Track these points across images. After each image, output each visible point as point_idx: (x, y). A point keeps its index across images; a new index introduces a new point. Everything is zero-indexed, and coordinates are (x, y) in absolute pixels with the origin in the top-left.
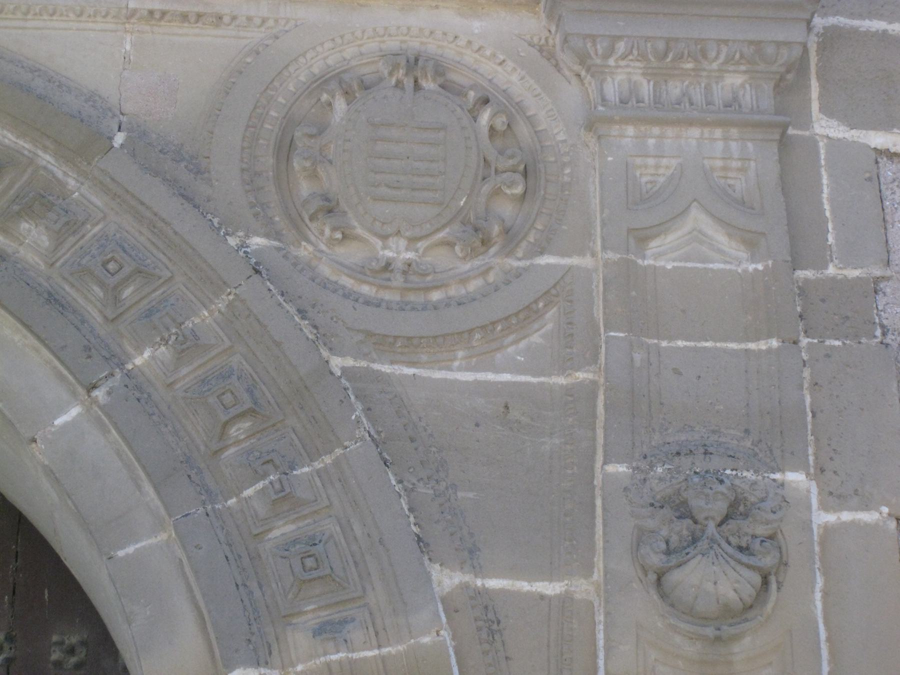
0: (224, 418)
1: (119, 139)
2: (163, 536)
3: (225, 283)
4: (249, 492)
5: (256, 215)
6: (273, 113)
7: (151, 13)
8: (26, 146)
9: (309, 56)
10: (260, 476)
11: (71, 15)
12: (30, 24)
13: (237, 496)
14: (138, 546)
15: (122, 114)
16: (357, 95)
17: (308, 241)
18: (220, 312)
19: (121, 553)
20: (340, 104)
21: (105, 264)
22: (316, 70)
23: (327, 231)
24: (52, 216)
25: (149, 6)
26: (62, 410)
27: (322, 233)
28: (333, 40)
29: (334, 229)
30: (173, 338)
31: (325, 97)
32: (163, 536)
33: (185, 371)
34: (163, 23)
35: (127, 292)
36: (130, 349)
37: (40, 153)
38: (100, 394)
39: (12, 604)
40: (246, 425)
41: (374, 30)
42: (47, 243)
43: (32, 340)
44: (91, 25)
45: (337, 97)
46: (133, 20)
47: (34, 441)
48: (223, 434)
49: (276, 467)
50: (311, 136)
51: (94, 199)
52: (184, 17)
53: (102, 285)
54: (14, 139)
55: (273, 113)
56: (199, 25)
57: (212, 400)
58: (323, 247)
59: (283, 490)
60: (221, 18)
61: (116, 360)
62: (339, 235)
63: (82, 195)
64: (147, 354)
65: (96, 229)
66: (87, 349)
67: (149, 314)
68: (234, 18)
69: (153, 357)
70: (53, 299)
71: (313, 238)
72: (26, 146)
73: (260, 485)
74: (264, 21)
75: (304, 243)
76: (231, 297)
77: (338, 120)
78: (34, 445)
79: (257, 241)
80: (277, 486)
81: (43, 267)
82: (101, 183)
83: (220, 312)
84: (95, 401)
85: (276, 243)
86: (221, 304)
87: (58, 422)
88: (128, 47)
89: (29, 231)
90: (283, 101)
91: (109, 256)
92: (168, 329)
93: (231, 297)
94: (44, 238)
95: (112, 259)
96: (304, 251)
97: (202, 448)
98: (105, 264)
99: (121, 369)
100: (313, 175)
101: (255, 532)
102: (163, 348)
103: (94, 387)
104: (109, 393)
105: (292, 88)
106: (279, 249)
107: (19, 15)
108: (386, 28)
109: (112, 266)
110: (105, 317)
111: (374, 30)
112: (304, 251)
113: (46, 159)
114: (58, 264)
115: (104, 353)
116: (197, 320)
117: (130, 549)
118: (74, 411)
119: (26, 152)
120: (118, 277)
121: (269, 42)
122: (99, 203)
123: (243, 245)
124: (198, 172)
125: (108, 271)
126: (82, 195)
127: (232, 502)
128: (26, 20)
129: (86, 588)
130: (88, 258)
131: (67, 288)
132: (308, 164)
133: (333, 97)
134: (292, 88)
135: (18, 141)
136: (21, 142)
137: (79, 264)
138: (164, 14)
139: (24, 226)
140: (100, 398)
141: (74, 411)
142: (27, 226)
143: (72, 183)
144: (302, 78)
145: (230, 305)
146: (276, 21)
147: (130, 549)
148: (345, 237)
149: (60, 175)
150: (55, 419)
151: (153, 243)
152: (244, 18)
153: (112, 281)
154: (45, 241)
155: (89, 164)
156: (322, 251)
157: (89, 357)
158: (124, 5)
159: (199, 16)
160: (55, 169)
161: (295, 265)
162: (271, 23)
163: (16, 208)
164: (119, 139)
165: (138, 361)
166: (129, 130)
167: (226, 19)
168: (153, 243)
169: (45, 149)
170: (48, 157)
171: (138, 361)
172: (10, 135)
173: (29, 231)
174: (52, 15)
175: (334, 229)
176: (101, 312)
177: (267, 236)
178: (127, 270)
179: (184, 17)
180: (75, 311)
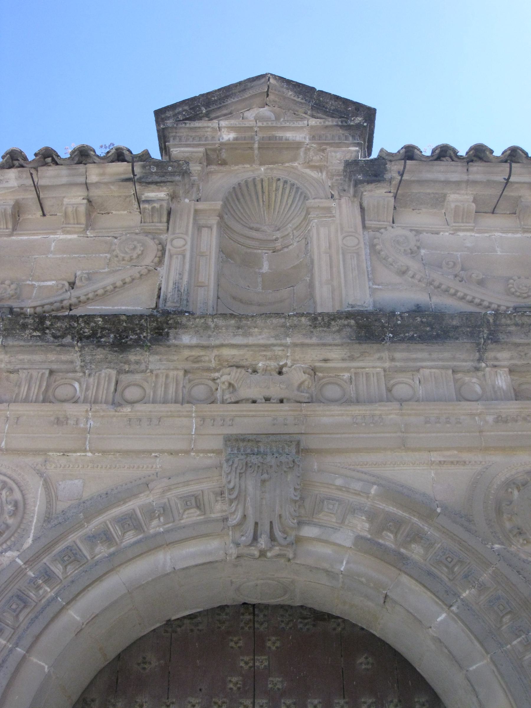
0: (501, 615)
1: (439, 510)
2: (485, 662)
3: (490, 563)
4: (515, 642)
5: (494, 536)
6: (491, 497)
7: (440, 462)
8: (407, 515)
9: (500, 475)
10: (518, 636)
11: (411, 464)
12: (396, 468)
13: (510, 644)
14: (477, 665)
15: (436, 500)
16: (521, 488)
17: (513, 545)
18: (490, 574)
19: (471, 669)
20: (516, 492)
21: (446, 558)
22: (503, 480)
23: (521, 541)
24: (422, 541)
25: (439, 459)
26: (439, 615)
27: (518, 541)
28: (507, 468)
29: (524, 540)
30: (477, 585)
31: (510, 490)
32: (485, 662)
33: (482, 597)
34: (444, 465)
35: (456, 569)
36: (460, 591)
37: (412, 517)
38: (454, 608)
39: (398, 687)
40: (509, 617)
41: (521, 463)
42: (423, 552)
43: (423, 589)
44: (418, 468)
45: (515, 490)
46: (433, 465)
47: (431, 627)
48: (501, 621)
49: (524, 633)
50: (508, 505)
51: (436, 534)
52: (452, 463)
53: (447, 567)
54: (402, 513)
55: (491, 497)
56: (458, 465)
57: (496, 608)
58: (519, 547)
59: (528, 641)
60: (465, 462)
61: (457, 595)
62: (525, 542)
63: (431, 533)
64: (467, 592)
65: (439, 545)
66: (446, 591)
67: (466, 576)
68: (470, 462)
69: (470, 593)
70: (430, 574)
71: (515, 543)
72: (407, 515)
73: (519, 640)
74: (481, 462)
75: (513, 546)
76: (494, 569)
77: (516, 498)
78: (430, 629)
79: (497, 546)
80: (526, 639)
81: (422, 561)
82: (438, 528)
83: (490, 574)
84: (452, 612)
85: (503, 546)
86: (490, 571)
87: (439, 620)
88: (433, 475)
89: (415, 548)
90: (494, 492)
91: (448, 556)
92: (474, 582)
93: (494, 569)
94: (422, 550)
95: (449, 557)
96: (513, 549)
97: (494, 627)
98: (446, 558)
99: (460, 598)
100: (510, 520)
101: (520, 657)
102: (473, 590)
103: (451, 606)
104: (458, 608)
105: (495, 487)
106: (505, 549)
107: (392, 465)
108: (525, 463)
109: (449, 560)
110: (449, 579)
111: (521, 463)
112: (513, 549)
113: (415, 520)
114: (428, 560)
115: (453, 593)
116: (483, 578)
117: (474, 667)
118: (444, 615)
119: (407, 518)
120: (452, 563)
121: (484, 470)
122: (438, 535)
123: (492, 548)
124: (470, 521)
125: (447, 561)
126: (431, 533)
127: (509, 646)
128: (394, 467)
129: (429, 681)
130: (439, 556)
131: (433, 569)
132: (509, 516)
133: (513, 490)
134: (495, 487)
135: (403, 514)
136: (404, 514)
137: (436, 559)
138: (444, 462)
139: (413, 546)
140: (454, 610)
141: (444, 615)
142: (414, 546)
143: (426, 528)
144: (499, 483)
145: (494, 572)
146: (485, 462)
147: (474, 667)
148: (527, 542)
149: (421, 525)
150: (438, 618)
151: (461, 550)
152: (474, 462)
153: (450, 565)
154: (422, 551)
155: (433, 521)
156: (519, 548)
157: (448, 594)
158: (430, 460)
159: (457, 462)
160: (419, 524)
161: (512, 554)
162: (483, 463)
163: (409, 539)
164: (439, 510)
165: (464, 595)
166: (441, 507)
167: (467, 463)
168: (461, 550)
169: (414, 516)
170: (415, 519)
171: (464, 595)
172: (400, 512)
173: (415, 548)
174: (404, 465)
175: (524, 540)
176: (447, 577)
177: (499, 544)
178: (455, 561)
179: (452, 463)
180: (438, 577)
